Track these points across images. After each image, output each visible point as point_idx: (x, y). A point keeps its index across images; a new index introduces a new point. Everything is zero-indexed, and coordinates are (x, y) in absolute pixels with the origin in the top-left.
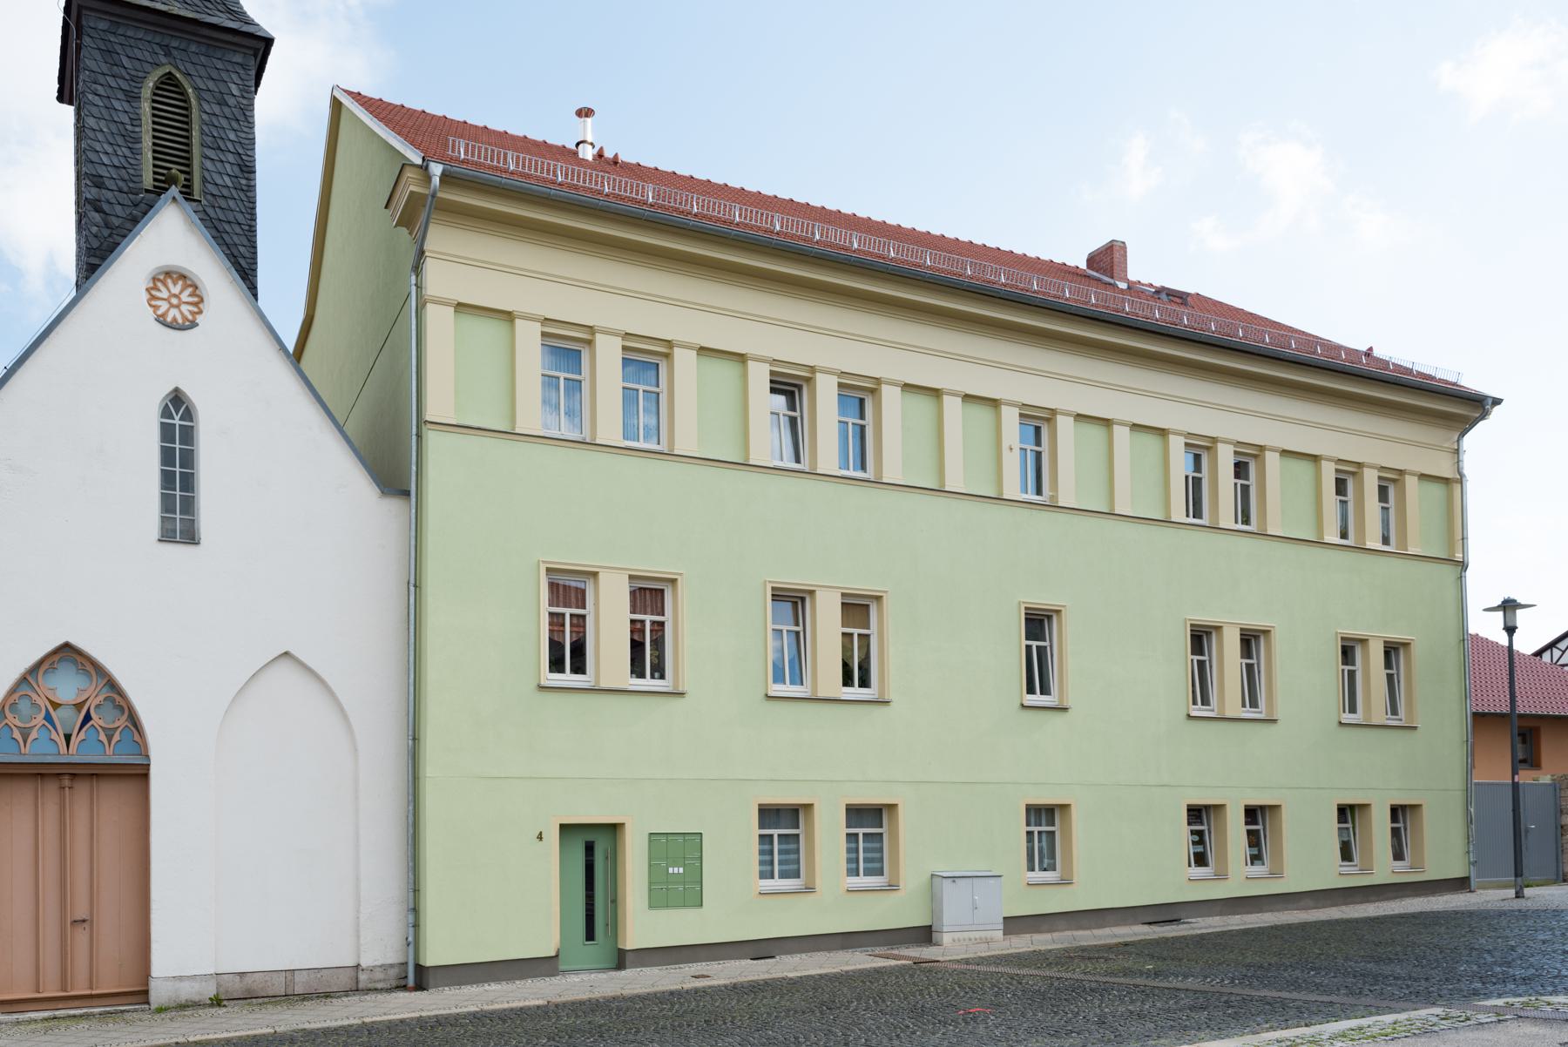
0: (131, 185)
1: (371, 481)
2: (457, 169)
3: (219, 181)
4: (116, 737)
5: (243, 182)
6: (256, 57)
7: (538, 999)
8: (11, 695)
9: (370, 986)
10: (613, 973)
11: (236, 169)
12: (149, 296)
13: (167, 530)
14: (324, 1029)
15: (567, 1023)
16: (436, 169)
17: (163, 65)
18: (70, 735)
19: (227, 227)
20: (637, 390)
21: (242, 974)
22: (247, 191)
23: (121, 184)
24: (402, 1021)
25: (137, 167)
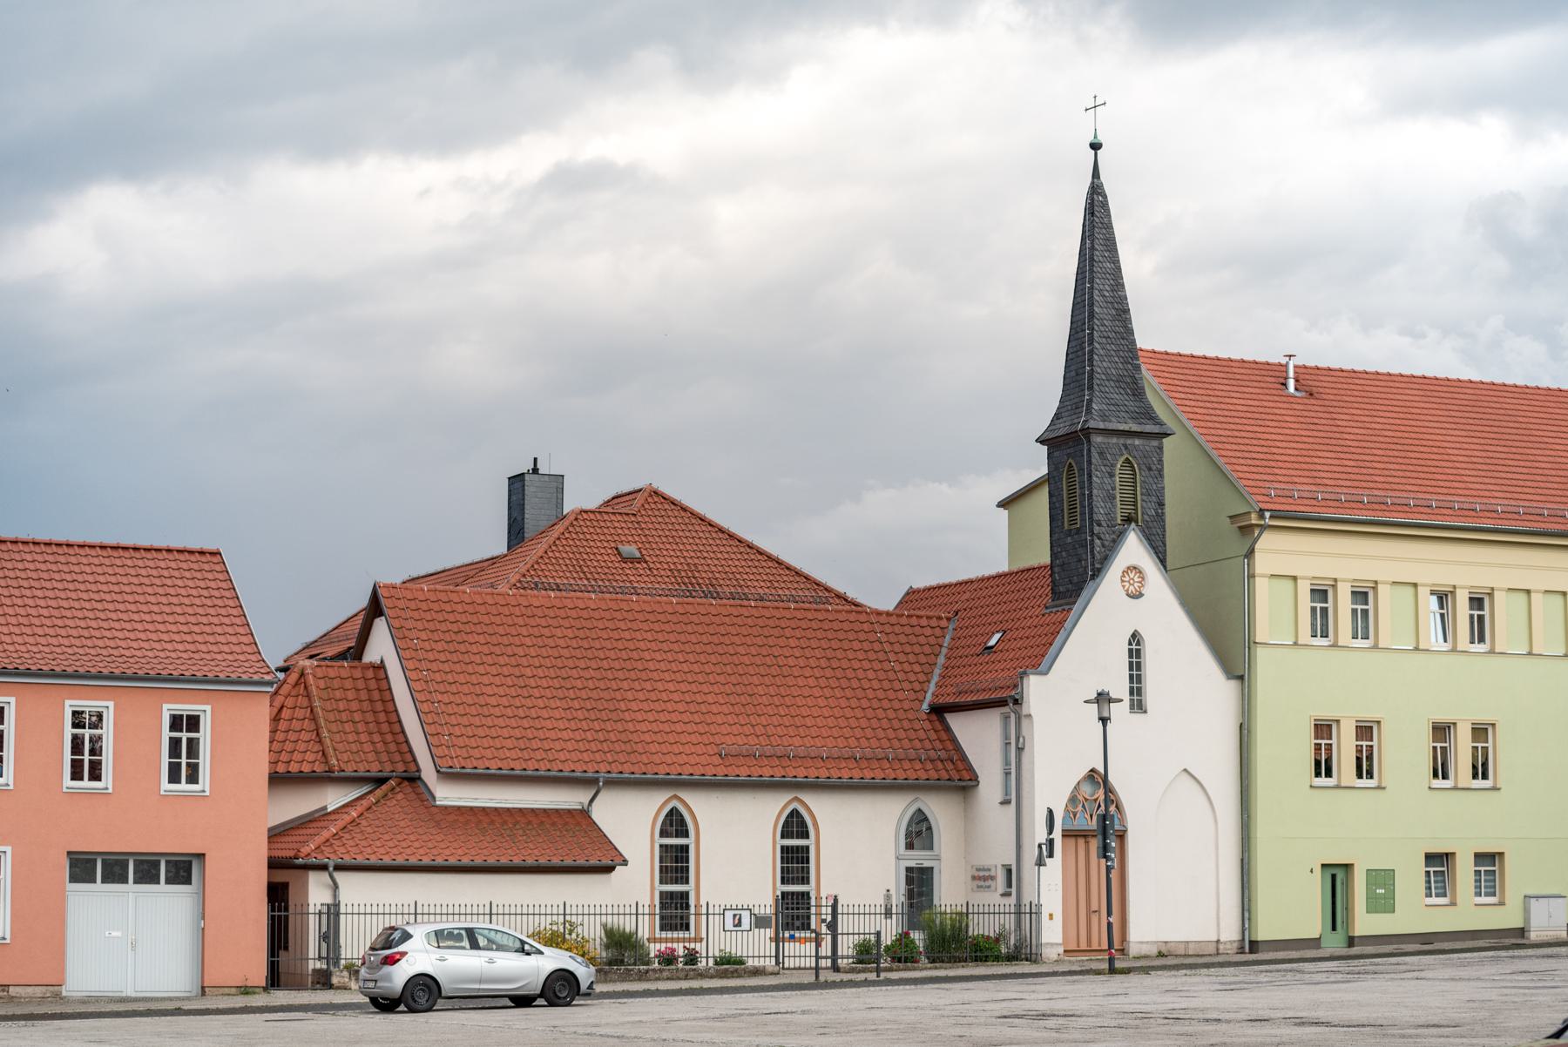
21: (1166, 942)
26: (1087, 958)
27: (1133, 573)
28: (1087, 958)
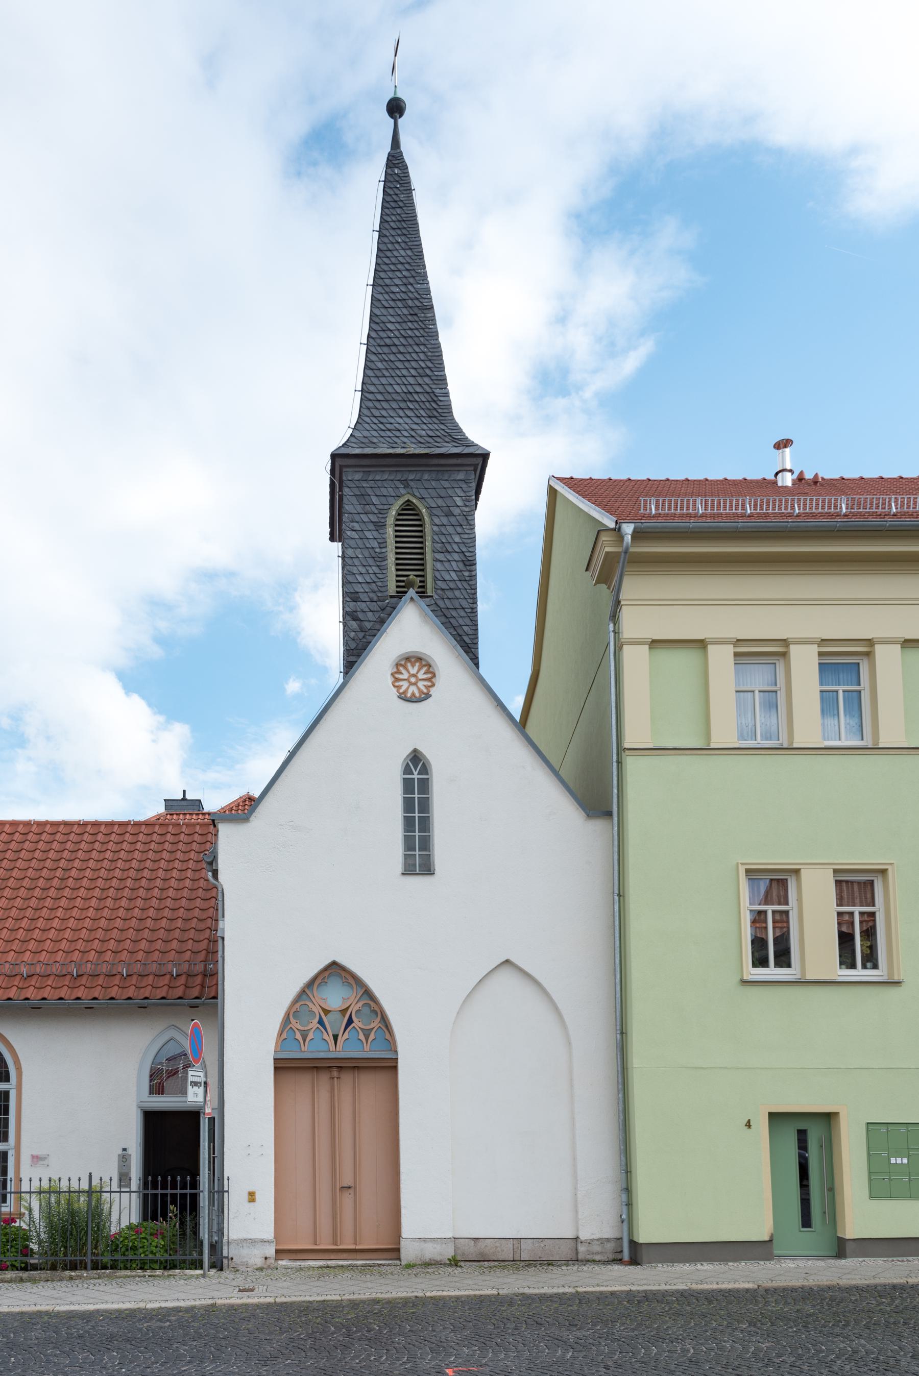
0: (379, 594)
1: (578, 806)
2: (647, 524)
3: (447, 577)
4: (372, 1037)
5: (466, 574)
6: (475, 471)
7: (748, 1282)
8: (294, 1005)
9: (589, 1257)
10: (832, 1262)
11: (461, 565)
12: (393, 679)
13: (409, 864)
14: (541, 1294)
15: (774, 1309)
16: (628, 529)
17: (403, 495)
18: (337, 1035)
19: (454, 613)
20: (837, 692)
21: (476, 1240)
22: (469, 581)
23: (372, 595)
24: (612, 1293)
25: (384, 580)
26: (321, 1263)
27: (416, 668)
28: (321, 1263)
